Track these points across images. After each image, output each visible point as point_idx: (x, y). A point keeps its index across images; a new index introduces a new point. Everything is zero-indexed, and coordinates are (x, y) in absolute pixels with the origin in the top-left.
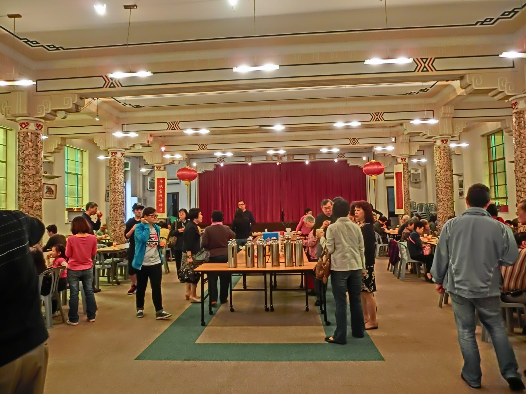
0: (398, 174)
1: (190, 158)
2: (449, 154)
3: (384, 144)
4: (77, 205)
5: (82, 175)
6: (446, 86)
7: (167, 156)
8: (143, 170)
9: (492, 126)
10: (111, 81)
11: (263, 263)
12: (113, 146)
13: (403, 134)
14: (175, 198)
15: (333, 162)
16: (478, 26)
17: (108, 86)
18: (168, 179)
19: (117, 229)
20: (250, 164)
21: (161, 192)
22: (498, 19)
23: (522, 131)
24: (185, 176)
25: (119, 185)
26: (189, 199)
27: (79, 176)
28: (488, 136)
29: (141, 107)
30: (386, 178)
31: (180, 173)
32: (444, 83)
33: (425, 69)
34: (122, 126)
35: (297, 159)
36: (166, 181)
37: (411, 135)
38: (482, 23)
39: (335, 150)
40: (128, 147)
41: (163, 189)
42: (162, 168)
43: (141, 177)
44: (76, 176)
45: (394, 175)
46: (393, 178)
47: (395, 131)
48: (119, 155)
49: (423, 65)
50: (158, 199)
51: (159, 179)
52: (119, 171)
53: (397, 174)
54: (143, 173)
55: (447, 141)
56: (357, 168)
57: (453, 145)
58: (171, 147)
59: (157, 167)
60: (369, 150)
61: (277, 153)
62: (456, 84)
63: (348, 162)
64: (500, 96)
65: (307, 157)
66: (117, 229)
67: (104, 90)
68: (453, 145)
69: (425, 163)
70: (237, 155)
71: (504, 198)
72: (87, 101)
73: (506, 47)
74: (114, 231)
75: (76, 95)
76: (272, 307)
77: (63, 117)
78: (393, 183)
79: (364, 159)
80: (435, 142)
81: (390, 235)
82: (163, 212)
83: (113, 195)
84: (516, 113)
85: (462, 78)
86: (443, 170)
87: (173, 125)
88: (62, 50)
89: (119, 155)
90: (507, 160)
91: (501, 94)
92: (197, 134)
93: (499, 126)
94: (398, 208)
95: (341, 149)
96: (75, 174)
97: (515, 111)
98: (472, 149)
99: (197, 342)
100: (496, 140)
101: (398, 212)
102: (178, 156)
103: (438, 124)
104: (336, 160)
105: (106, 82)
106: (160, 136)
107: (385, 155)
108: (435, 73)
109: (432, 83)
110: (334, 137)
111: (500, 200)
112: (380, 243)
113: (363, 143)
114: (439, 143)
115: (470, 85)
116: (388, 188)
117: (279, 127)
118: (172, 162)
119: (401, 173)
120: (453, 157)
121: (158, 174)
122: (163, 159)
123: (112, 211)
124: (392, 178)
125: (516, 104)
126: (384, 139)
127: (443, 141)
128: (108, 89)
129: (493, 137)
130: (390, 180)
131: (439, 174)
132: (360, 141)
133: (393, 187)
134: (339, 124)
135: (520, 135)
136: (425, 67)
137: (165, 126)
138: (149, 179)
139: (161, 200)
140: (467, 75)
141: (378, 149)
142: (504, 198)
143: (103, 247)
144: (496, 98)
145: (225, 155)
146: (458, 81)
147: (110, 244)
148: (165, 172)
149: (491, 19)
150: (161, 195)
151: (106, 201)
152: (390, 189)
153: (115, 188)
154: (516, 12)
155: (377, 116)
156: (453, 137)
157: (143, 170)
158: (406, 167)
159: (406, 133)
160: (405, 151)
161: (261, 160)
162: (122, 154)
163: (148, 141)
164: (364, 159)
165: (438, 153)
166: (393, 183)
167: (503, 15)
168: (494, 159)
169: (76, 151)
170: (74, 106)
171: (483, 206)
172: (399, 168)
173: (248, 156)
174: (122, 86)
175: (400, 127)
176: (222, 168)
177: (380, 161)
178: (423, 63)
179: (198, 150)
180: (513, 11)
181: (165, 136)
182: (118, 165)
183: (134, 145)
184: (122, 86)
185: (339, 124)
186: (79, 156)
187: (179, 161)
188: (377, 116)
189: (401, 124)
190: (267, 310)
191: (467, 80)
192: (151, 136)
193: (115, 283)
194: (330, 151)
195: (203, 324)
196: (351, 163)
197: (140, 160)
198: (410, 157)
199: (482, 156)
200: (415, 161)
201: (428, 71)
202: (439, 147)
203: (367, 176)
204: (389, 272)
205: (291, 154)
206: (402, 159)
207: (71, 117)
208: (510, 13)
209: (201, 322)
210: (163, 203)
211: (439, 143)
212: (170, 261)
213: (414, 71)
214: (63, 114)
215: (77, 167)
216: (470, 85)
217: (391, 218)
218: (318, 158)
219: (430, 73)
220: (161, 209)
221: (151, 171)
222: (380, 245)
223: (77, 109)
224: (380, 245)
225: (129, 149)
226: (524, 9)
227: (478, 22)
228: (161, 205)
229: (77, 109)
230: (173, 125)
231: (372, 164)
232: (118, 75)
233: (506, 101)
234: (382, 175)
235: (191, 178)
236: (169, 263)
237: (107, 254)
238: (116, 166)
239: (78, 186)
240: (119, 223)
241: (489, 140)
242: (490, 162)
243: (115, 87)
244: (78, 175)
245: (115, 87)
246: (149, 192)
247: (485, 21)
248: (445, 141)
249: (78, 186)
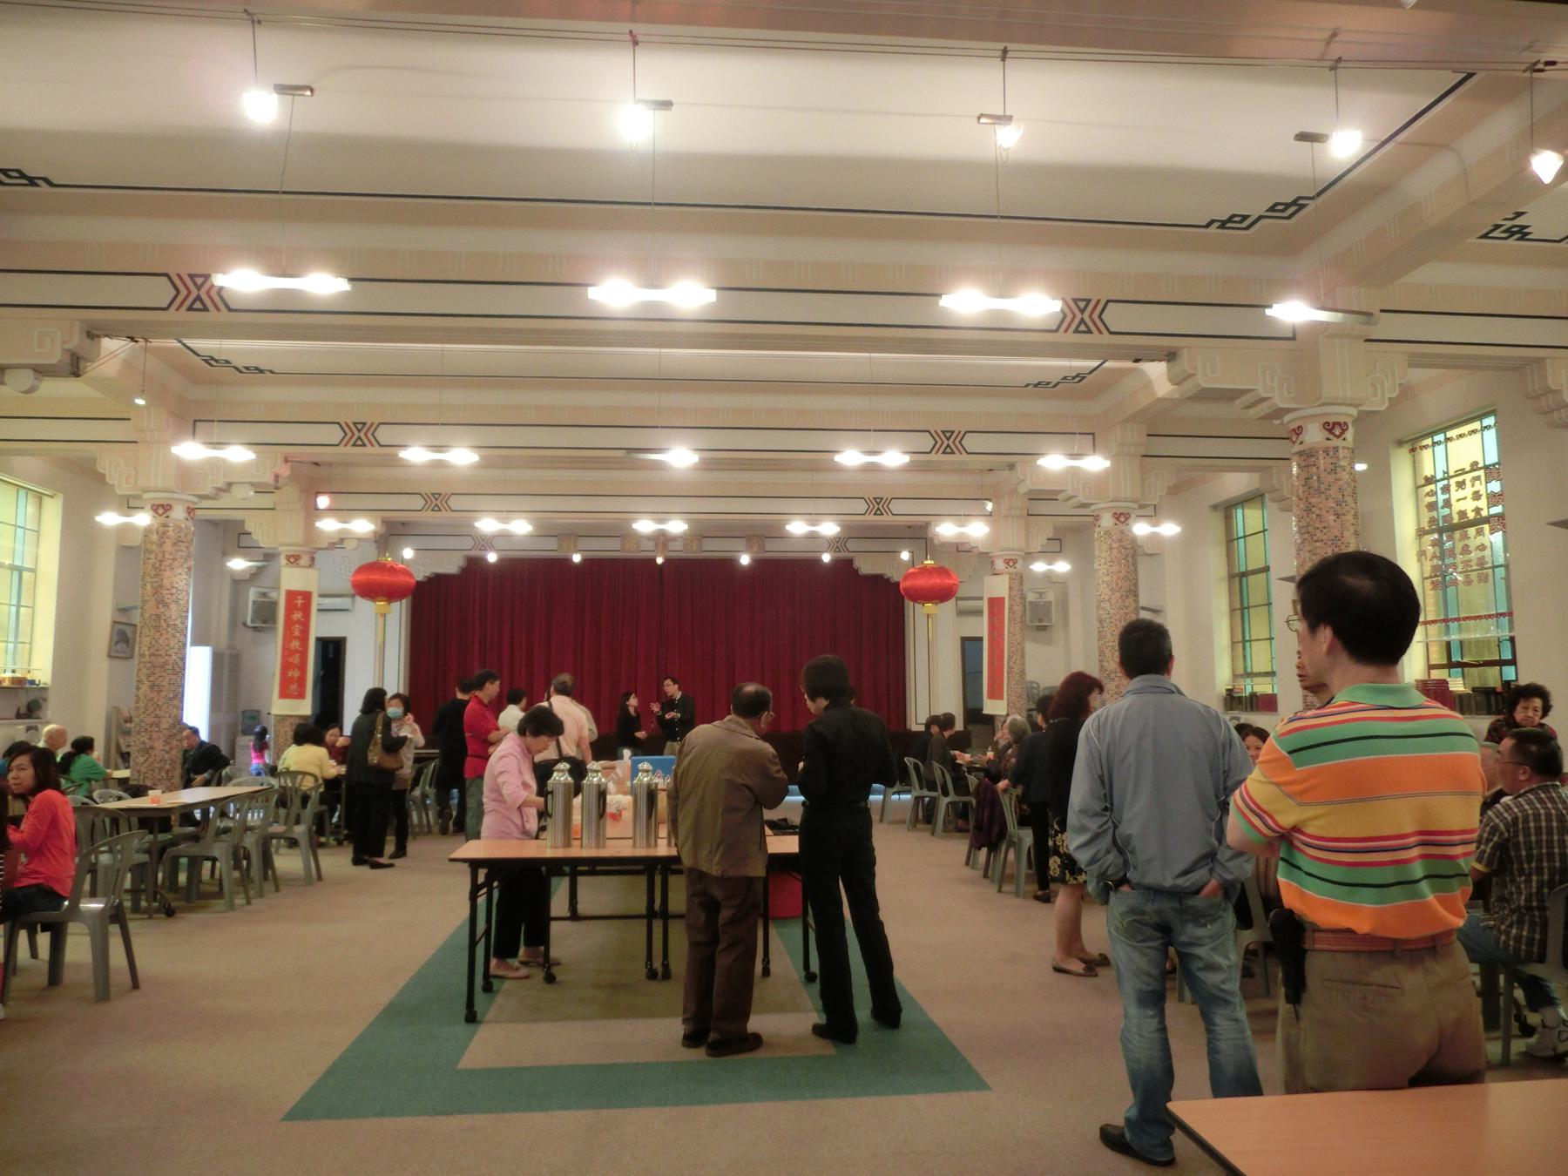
0: (996, 604)
1: (393, 532)
2: (1132, 554)
3: (961, 518)
4: (10, 666)
5: (33, 571)
6: (1133, 370)
7: (328, 525)
8: (238, 564)
9: (1236, 483)
10: (194, 293)
11: (648, 837)
12: (160, 485)
13: (1015, 491)
14: (332, 654)
15: (819, 561)
16: (1213, 229)
17: (187, 304)
18: (321, 596)
19: (159, 745)
20: (745, 560)
21: (297, 633)
22: (1260, 218)
23: (1313, 501)
24: (375, 585)
25: (173, 606)
26: (377, 657)
27: (25, 574)
28: (1227, 509)
29: (261, 371)
30: (961, 613)
31: (362, 577)
32: (1130, 364)
33: (1083, 328)
34: (193, 420)
35: (714, 549)
36: (316, 602)
37: (1036, 497)
38: (1223, 224)
39: (829, 529)
40: (208, 491)
41: (305, 625)
42: (304, 560)
43: (227, 586)
44: (16, 574)
45: (985, 605)
46: (980, 613)
47: (991, 482)
48: (178, 513)
49: (1086, 316)
50: (287, 653)
51: (291, 595)
52: (176, 564)
53: (992, 601)
54: (232, 573)
55: (1127, 516)
56: (879, 581)
57: (1141, 529)
58: (349, 497)
59: (288, 558)
60: (918, 535)
61: (658, 528)
62: (1156, 371)
63: (856, 564)
64: (1263, 409)
65: (740, 544)
66: (159, 745)
67: (171, 315)
68: (1141, 529)
69: (1066, 576)
70: (543, 532)
71: (1267, 674)
72: (108, 344)
73: (1280, 287)
74: (147, 750)
75: (77, 324)
76: (666, 966)
77: (26, 388)
78: (980, 627)
79: (905, 555)
80: (1097, 518)
81: (971, 769)
82: (301, 695)
83: (137, 642)
84: (1301, 454)
85: (1170, 356)
86: (1118, 595)
87: (359, 432)
88: (45, 188)
89: (178, 513)
90: (1274, 574)
91: (1264, 405)
92: (439, 464)
93: (1256, 485)
94: (992, 696)
95: (846, 528)
96: (13, 568)
97: (1297, 448)
98: (1186, 543)
99: (464, 1063)
100: (1249, 519)
101: (991, 707)
102: (363, 526)
103: (1106, 472)
104: (826, 558)
105: (178, 291)
106: (316, 464)
107: (960, 549)
108: (1106, 339)
109: (1095, 363)
110: (822, 486)
111: (1256, 680)
112: (946, 793)
113: (904, 512)
114: (1107, 521)
115: (1190, 376)
116: (964, 640)
117: (680, 457)
118: (339, 542)
119: (194, 643)
120: (1141, 561)
121: (292, 579)
122: (310, 531)
123: (145, 688)
124: (979, 612)
125: (1298, 431)
126: (966, 501)
127: (1117, 516)
128: (184, 315)
129: (1239, 511)
130: (972, 620)
131: (1106, 605)
132: (896, 507)
133: (981, 639)
134: (850, 457)
135: (1308, 510)
136: (1082, 321)
137: (334, 434)
138: (252, 594)
139: (296, 659)
140: (1185, 351)
141: (946, 530)
142: (1267, 674)
143: (120, 798)
144: (1252, 412)
145: (505, 529)
146: (1163, 365)
147: (138, 792)
148: (312, 574)
149: (1245, 217)
150: (295, 644)
151: (110, 656)
152: (970, 646)
153: (158, 616)
154: (1303, 206)
155: (948, 441)
156: (1142, 507)
157: (238, 564)
158: (1016, 586)
159: (1023, 489)
160: (1013, 539)
161: (609, 548)
162: (190, 511)
163: (277, 477)
164: (905, 555)
165: (1105, 547)
166: (980, 627)
167: (1272, 209)
168: (1243, 569)
169: (22, 492)
170: (67, 359)
171: (994, 792)
172: (999, 586)
173: (572, 535)
174: (230, 310)
175: (1006, 473)
176: (495, 566)
177: (946, 565)
178: (1085, 316)
179: (425, 507)
180: (1294, 203)
181: (330, 464)
182: (174, 544)
183: (230, 484)
184: (230, 310)
185: (850, 457)
186: (31, 509)
187: (359, 540)
188: (948, 441)
189: (1012, 467)
190: (652, 975)
191: (1184, 363)
192: (286, 461)
193: (157, 911)
194: (812, 530)
195: (472, 1018)
196: (866, 566)
197: (231, 535)
198: (1030, 557)
199: (1214, 564)
200: (1039, 567)
201: (1089, 332)
202: (1107, 533)
203: (909, 604)
204: (967, 872)
205: (700, 533)
206: (1007, 562)
207: (54, 388)
208: (1288, 206)
209: (464, 1012)
210: (302, 667)
211: (1107, 521)
212: (322, 845)
213: (1057, 331)
214: (28, 378)
215: (19, 547)
216: (1190, 376)
217: (970, 727)
218: (774, 550)
219: (1094, 338)
220: (294, 687)
221: (260, 570)
222: (948, 800)
223: (75, 366)
224: (948, 800)
225: (213, 498)
226: (1319, 200)
227: (1212, 222)
228: (295, 674)
229: (75, 366)
230: (359, 432)
231: (926, 571)
232: (243, 281)
233: (1277, 422)
234: (949, 606)
235: (391, 594)
236: (320, 852)
237: (192, 814)
238: (168, 547)
239: (18, 606)
240: (164, 725)
241: (1228, 520)
242: (1231, 576)
243: (205, 309)
244: (20, 570)
245: (205, 309)
246: (249, 633)
247: (1230, 220)
248: (1122, 517)
249: (18, 606)
